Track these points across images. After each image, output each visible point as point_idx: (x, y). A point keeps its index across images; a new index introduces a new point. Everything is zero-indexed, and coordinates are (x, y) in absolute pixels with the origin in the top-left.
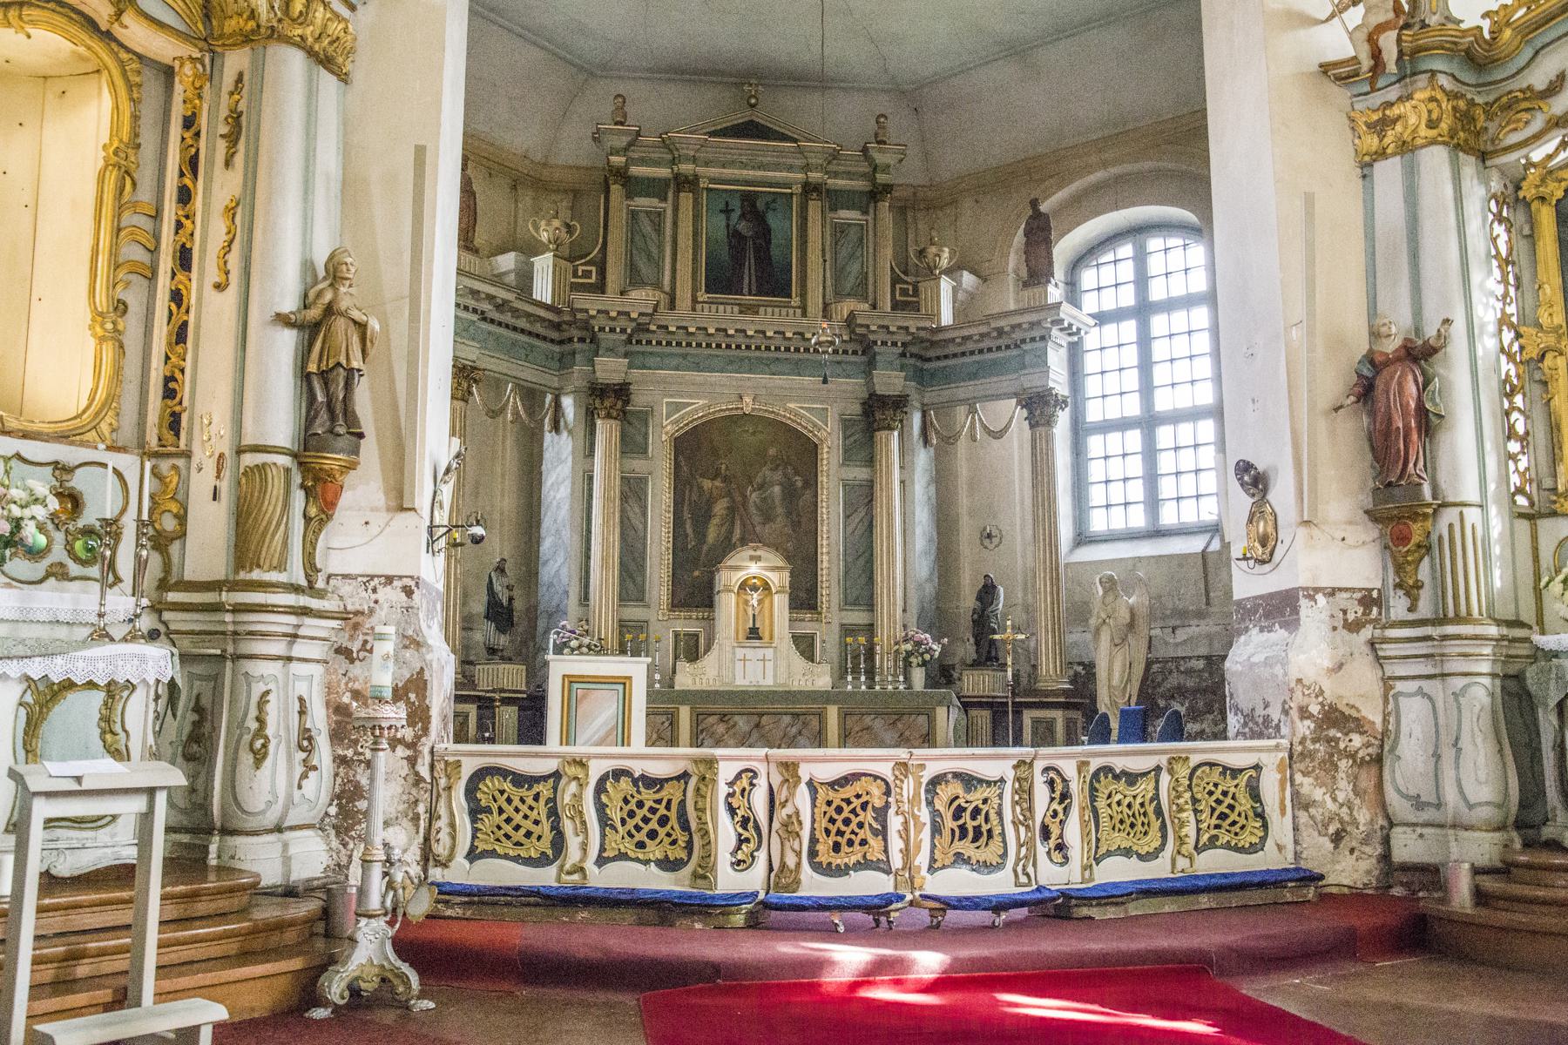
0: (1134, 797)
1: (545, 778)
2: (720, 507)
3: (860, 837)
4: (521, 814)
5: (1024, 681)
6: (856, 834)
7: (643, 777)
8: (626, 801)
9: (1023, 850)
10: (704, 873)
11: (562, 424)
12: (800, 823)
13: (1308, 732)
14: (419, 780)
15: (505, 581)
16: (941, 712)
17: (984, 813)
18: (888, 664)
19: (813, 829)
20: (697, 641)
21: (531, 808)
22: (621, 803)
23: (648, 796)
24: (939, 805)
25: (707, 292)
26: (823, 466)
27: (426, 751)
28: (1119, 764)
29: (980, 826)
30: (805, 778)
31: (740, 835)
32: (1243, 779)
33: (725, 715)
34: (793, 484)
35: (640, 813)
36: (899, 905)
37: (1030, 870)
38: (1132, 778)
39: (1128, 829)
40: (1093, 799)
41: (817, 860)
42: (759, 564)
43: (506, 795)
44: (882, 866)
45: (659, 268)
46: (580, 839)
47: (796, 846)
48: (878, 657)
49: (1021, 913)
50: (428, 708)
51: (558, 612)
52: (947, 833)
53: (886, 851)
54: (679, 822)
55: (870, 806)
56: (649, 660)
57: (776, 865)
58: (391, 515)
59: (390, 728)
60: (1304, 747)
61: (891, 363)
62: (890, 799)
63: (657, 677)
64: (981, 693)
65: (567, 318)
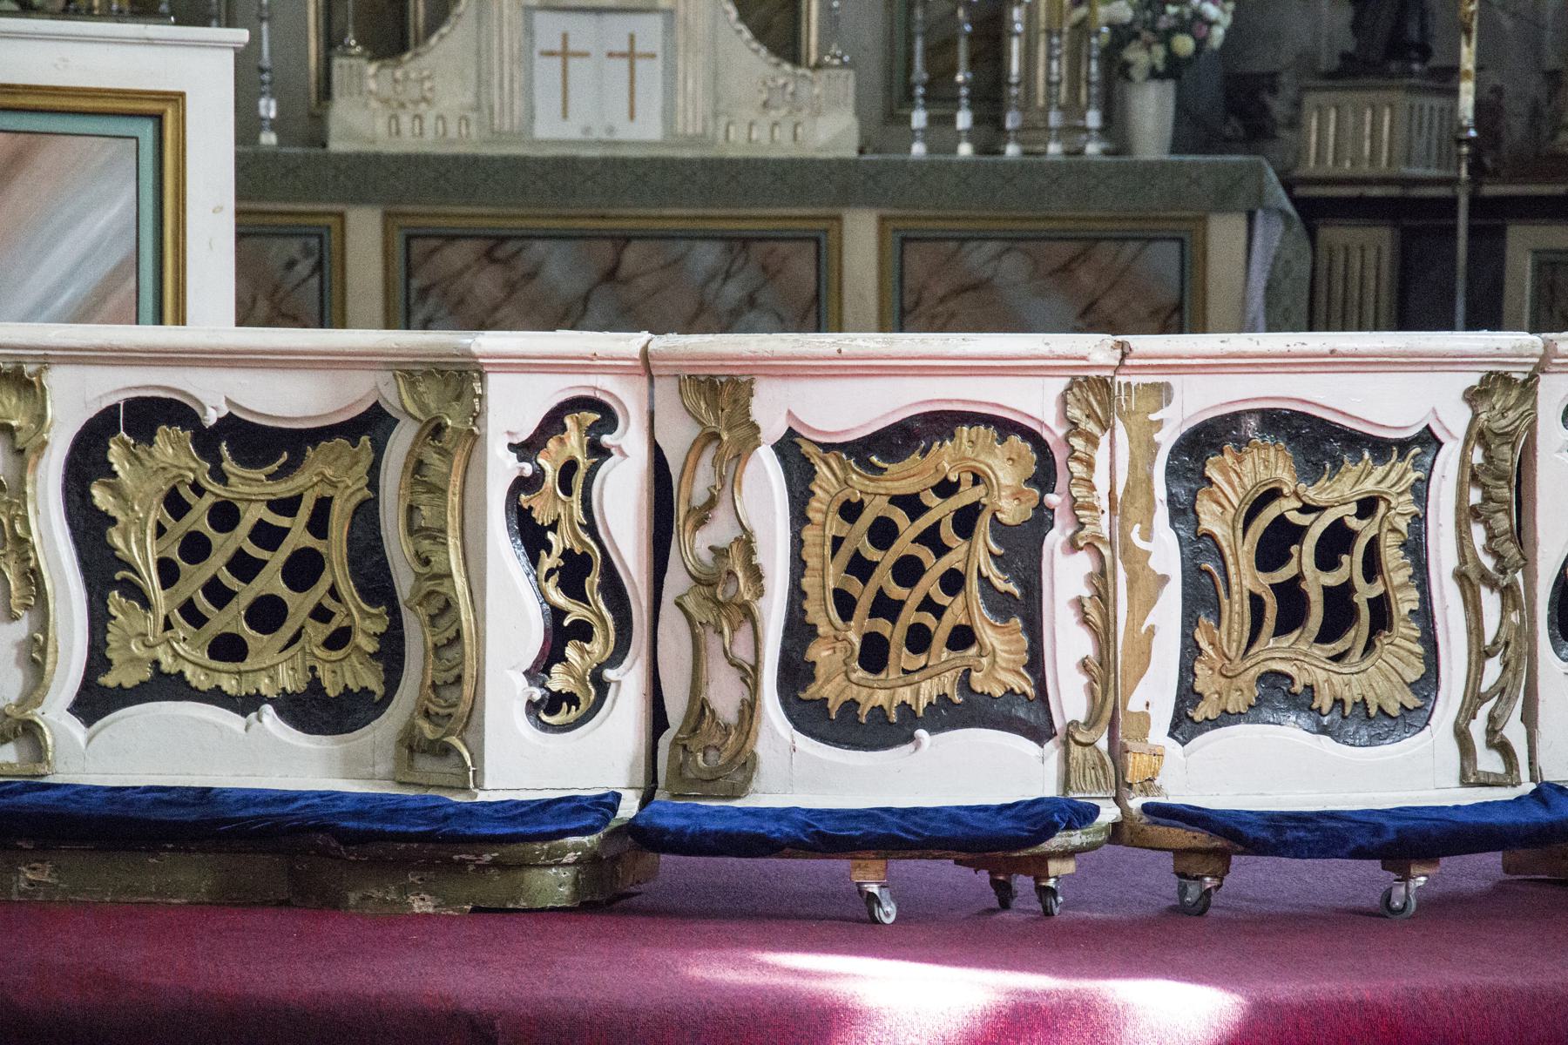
3: (949, 621)
5: (1515, 128)
6: (939, 611)
8: (176, 505)
9: (1493, 670)
12: (756, 574)
17: (1360, 546)
18: (1052, 69)
19: (797, 595)
22: (158, 512)
24: (1212, 519)
29: (1348, 588)
30: (773, 428)
31: (557, 614)
33: (503, 239)
35: (224, 545)
36: (1077, 838)
37: (1514, 732)
41: (812, 692)
44: (1021, 713)
47: (743, 652)
48: (1015, 46)
49: (1487, 866)
52: (1236, 610)
53: (1035, 664)
54: (355, 574)
55: (984, 522)
56: (242, 35)
57: (676, 708)
62: (1052, 499)
63: (268, 108)
64: (1365, 169)
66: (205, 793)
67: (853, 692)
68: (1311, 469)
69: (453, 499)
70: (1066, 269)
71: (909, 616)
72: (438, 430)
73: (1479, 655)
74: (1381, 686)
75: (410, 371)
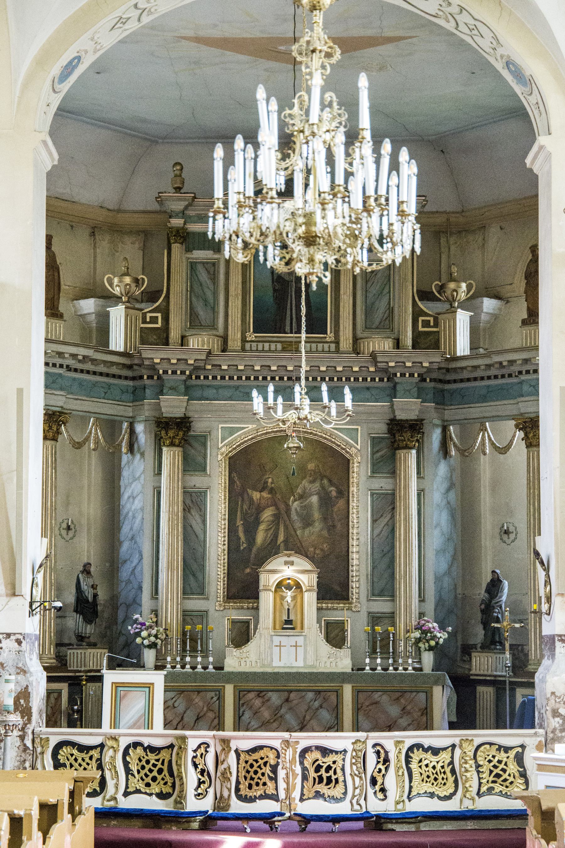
0: (438, 762)
1: (95, 747)
2: (267, 514)
4: (82, 767)
7: (149, 747)
8: (140, 760)
9: (357, 792)
10: (181, 800)
11: (136, 446)
12: (230, 773)
13: (557, 725)
14: (26, 748)
15: (90, 581)
16: (437, 691)
19: (238, 776)
20: (248, 627)
21: (88, 764)
22: (137, 761)
23: (152, 757)
25: (255, 332)
26: (354, 478)
27: (30, 732)
28: (427, 743)
29: (331, 776)
30: (234, 748)
31: (200, 779)
32: (512, 754)
34: (328, 494)
35: (148, 767)
37: (362, 802)
38: (435, 751)
39: (433, 781)
40: (408, 762)
41: (240, 793)
42: (292, 568)
43: (74, 757)
45: (214, 310)
46: (115, 781)
47: (229, 786)
49: (360, 824)
50: (31, 708)
51: (135, 603)
52: (311, 780)
53: (277, 789)
55: (268, 764)
57: (218, 797)
58: (8, 598)
59: (13, 725)
60: (555, 734)
61: (409, 391)
64: (486, 673)
65: (136, 361)
66: (142, 810)
67: (247, 793)
68: (324, 756)
69: (183, 759)
70: (398, 699)
71: (256, 780)
72: (181, 748)
73: (355, 788)
74: (337, 794)
75: (178, 738)
